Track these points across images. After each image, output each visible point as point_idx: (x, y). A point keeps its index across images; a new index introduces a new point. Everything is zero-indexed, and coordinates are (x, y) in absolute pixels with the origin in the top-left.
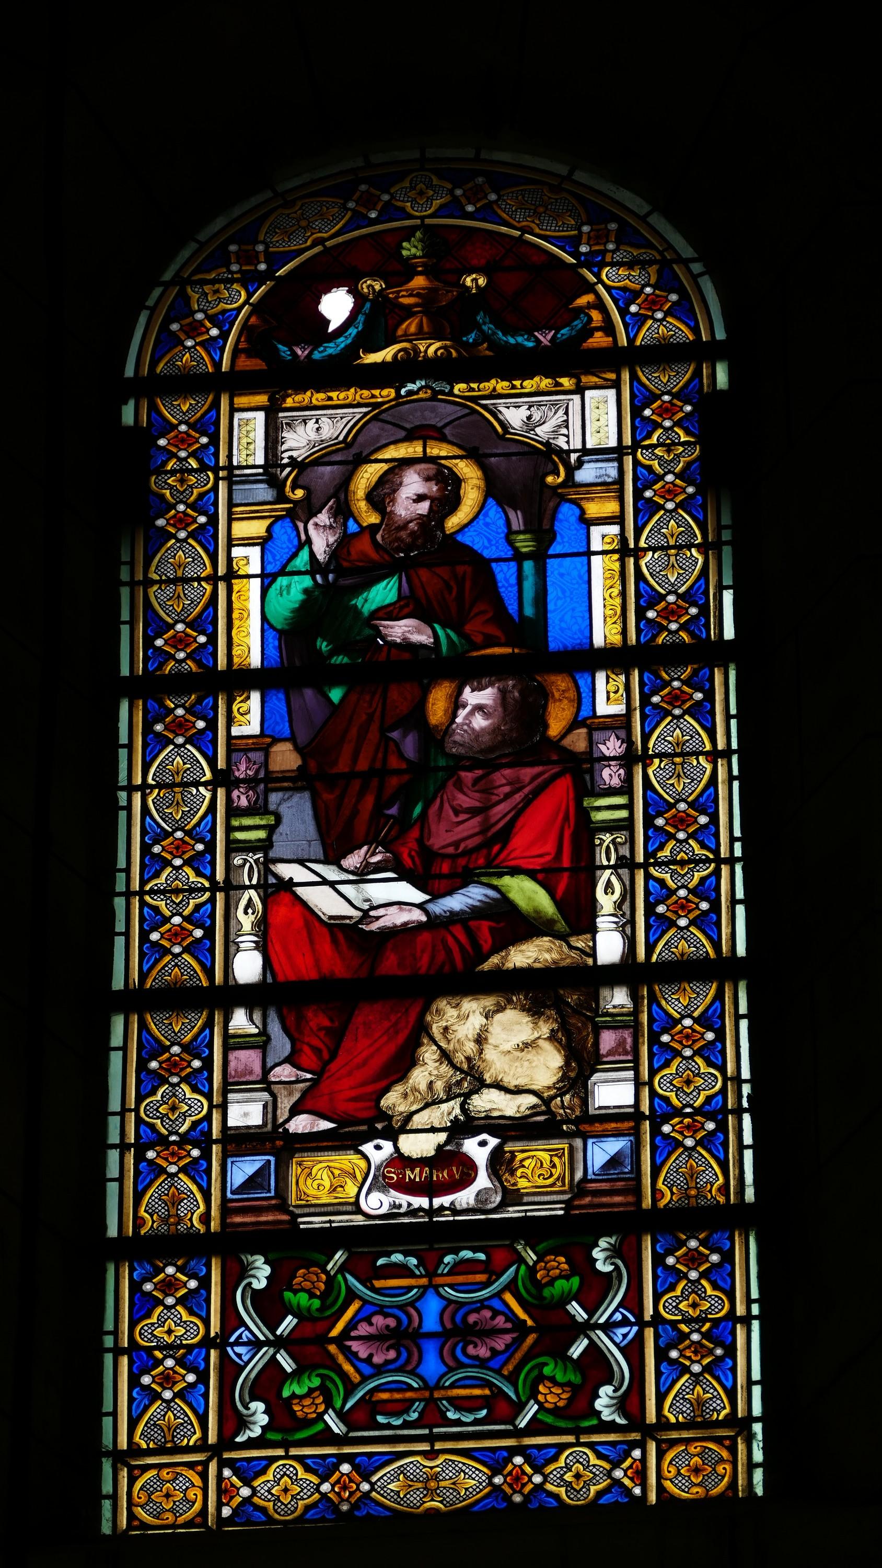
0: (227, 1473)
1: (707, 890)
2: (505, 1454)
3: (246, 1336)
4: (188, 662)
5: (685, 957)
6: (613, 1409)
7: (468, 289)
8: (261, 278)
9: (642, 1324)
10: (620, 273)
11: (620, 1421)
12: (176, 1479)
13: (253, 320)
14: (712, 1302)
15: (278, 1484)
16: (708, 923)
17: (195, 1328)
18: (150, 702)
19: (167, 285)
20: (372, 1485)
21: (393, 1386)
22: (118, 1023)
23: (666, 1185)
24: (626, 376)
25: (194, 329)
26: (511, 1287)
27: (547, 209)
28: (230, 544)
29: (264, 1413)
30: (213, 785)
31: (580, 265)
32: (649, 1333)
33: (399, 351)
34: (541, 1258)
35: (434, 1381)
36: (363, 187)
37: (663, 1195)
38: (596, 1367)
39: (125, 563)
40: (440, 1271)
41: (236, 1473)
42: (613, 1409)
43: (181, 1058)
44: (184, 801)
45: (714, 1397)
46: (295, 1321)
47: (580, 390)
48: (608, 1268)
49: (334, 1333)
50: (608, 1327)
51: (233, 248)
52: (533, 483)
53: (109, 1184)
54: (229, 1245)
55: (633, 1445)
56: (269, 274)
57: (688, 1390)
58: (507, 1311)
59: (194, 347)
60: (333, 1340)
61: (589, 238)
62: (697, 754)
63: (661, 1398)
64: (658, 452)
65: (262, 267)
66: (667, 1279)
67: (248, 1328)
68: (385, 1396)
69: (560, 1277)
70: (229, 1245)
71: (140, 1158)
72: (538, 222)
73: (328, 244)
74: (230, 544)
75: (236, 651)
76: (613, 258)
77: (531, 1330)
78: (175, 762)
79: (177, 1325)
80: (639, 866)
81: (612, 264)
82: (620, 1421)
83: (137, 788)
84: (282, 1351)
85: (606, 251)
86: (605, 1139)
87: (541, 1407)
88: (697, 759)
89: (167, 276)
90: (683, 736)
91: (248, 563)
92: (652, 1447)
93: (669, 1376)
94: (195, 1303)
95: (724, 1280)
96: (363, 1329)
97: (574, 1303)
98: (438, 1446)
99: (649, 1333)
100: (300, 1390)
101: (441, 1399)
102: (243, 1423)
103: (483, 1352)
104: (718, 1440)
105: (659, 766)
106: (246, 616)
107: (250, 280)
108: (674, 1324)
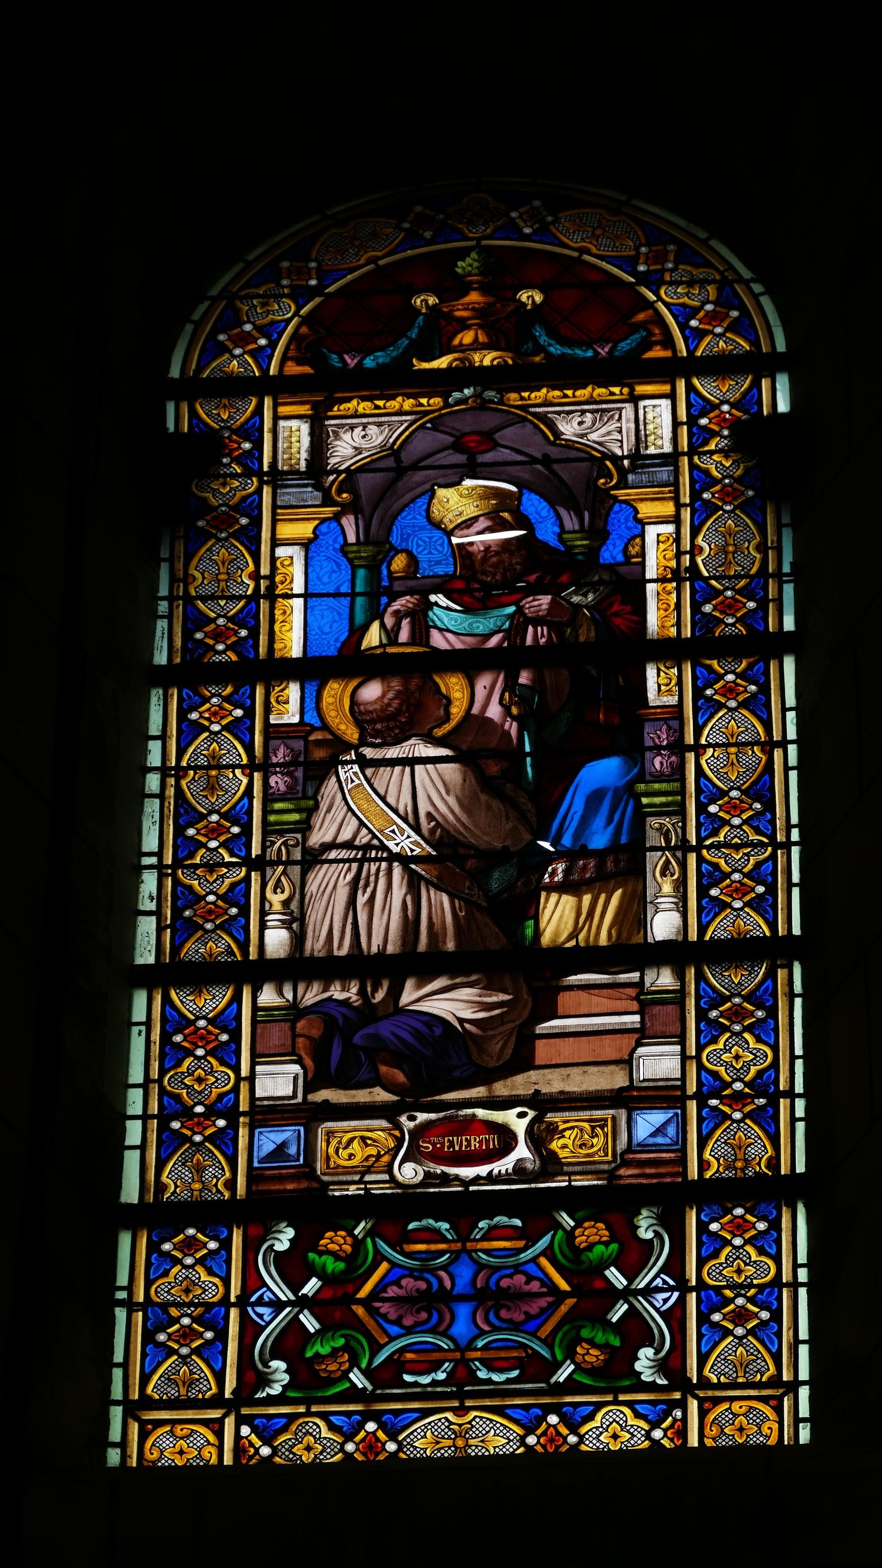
0: (245, 1430)
1: (763, 874)
2: (539, 1412)
3: (268, 1296)
4: (228, 653)
5: (742, 936)
6: (654, 1370)
7: (524, 305)
8: (311, 293)
9: (682, 1286)
10: (679, 290)
11: (662, 1381)
12: (190, 1435)
13: (304, 330)
14: (758, 1268)
15: (607, 1431)
16: (764, 906)
17: (214, 1288)
18: (185, 691)
19: (215, 300)
20: (400, 1444)
21: (499, 1344)
22: (140, 999)
23: (713, 1156)
24: (681, 385)
25: (244, 340)
26: (548, 1252)
27: (604, 231)
28: (275, 542)
29: (285, 1371)
30: (250, 768)
31: (639, 283)
32: (692, 1298)
33: (455, 360)
34: (579, 1224)
35: (465, 1343)
36: (419, 208)
37: (709, 1164)
38: (636, 1331)
39: (165, 560)
40: (472, 1237)
41: (254, 1430)
42: (654, 1370)
43: (207, 1030)
44: (738, 762)
45: (201, 1378)
46: (320, 1283)
47: (634, 399)
48: (649, 1235)
49: (363, 1293)
50: (648, 1292)
51: (285, 264)
52: (590, 485)
53: (127, 1153)
54: (255, 1212)
55: (672, 1405)
56: (317, 291)
57: (730, 1352)
58: (541, 1275)
59: (242, 355)
60: (360, 1302)
61: (647, 258)
62: (233, 767)
63: (702, 1359)
64: (715, 457)
65: (313, 282)
66: (711, 1246)
67: (270, 1289)
68: (409, 1356)
69: (600, 1242)
70: (255, 1212)
71: (163, 1127)
72: (595, 243)
73: (381, 262)
74: (275, 542)
75: (277, 646)
76: (671, 277)
77: (565, 1295)
78: (212, 748)
79: (746, 1264)
80: (692, 849)
81: (670, 283)
82: (662, 1381)
83: (690, 748)
84: (306, 1312)
85: (664, 270)
86: (649, 1111)
87: (578, 1368)
88: (233, 772)
89: (214, 292)
90: (738, 727)
91: (292, 563)
92: (693, 1405)
93: (709, 1338)
94: (216, 1263)
95: (220, 1267)
96: (392, 1291)
97: (612, 1269)
98: (469, 1403)
99: (692, 1298)
100: (325, 1350)
101: (473, 1360)
102: (265, 1380)
103: (519, 1317)
104: (764, 1400)
105: (713, 756)
106: (288, 612)
107: (300, 296)
108: (718, 1290)
